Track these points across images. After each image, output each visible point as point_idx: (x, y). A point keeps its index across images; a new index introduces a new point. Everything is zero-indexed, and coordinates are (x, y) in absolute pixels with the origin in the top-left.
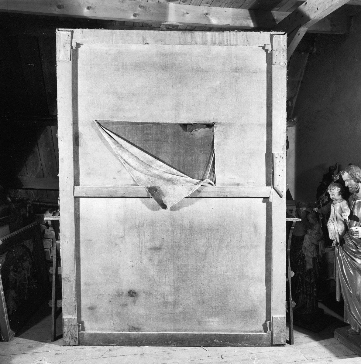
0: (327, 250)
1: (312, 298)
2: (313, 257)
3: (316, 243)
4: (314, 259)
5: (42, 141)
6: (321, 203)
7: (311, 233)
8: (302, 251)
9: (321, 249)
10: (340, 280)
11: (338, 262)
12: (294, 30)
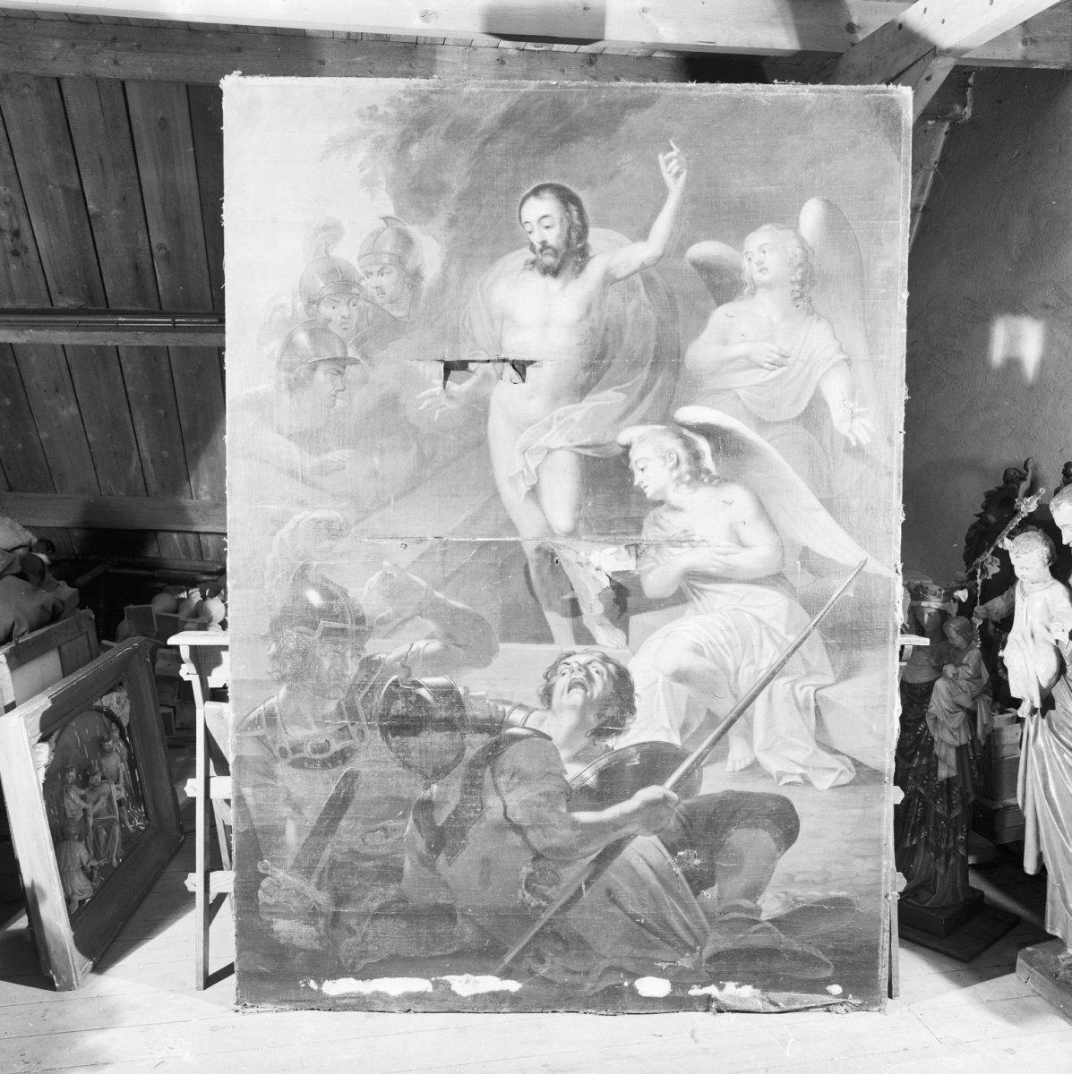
0: (1000, 720)
1: (952, 861)
2: (957, 744)
3: (968, 704)
4: (960, 750)
5: (203, 464)
6: (980, 577)
7: (954, 675)
8: (926, 728)
9: (982, 722)
10: (1039, 814)
11: (1032, 761)
12: (916, 62)
